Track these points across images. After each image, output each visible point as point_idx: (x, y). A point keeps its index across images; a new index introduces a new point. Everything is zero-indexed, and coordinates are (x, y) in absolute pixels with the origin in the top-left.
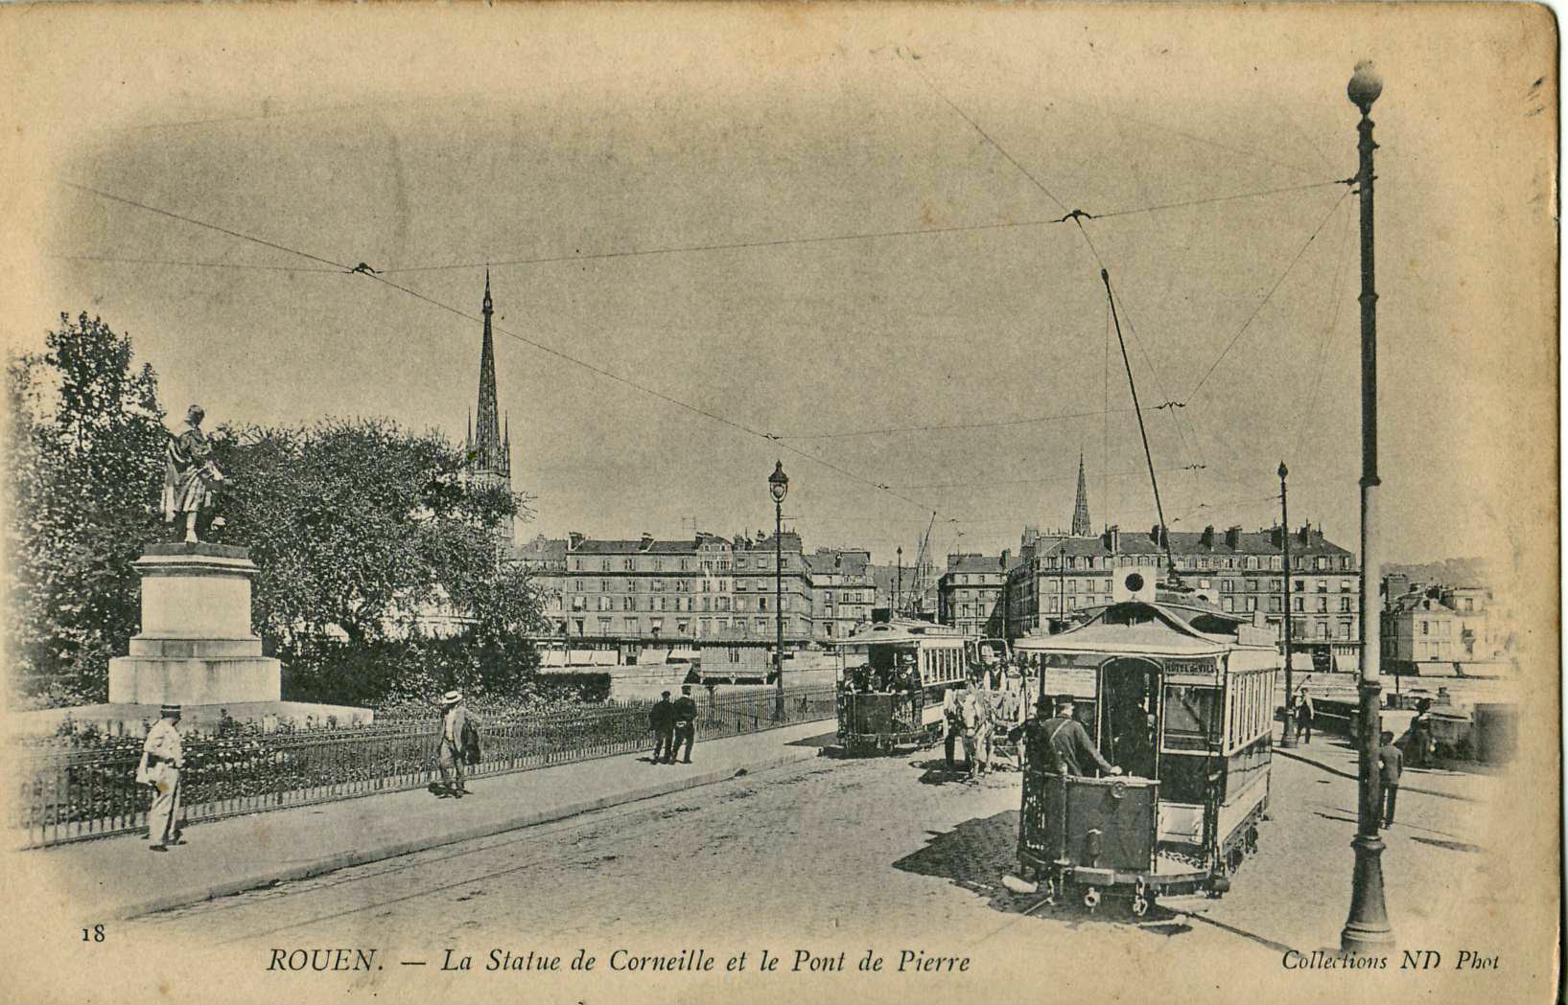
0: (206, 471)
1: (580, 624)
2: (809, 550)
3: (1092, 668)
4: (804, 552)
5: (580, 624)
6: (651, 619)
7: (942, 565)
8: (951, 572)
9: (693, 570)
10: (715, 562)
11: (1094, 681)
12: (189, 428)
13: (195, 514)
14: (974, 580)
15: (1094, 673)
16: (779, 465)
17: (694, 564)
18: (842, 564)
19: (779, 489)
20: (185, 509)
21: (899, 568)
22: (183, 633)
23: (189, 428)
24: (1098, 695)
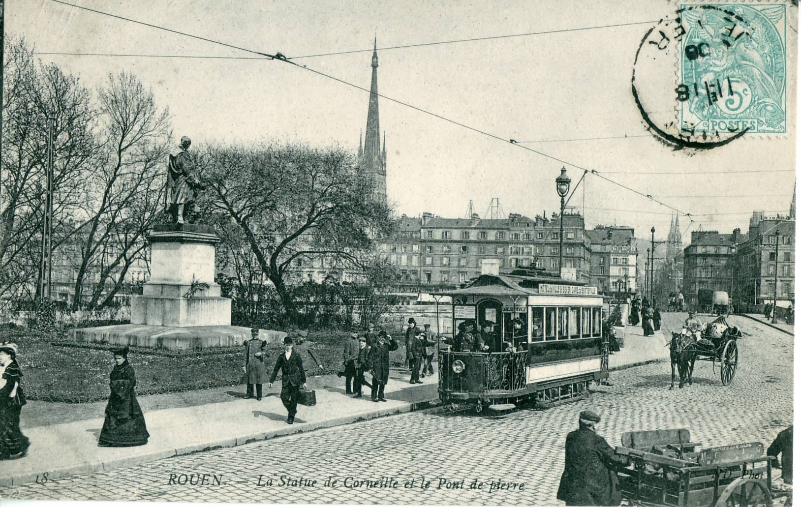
0: (190, 178)
1: (429, 276)
2: (589, 227)
3: (473, 305)
4: (586, 228)
5: (429, 276)
6: (441, 272)
7: (687, 240)
8: (694, 243)
9: (507, 239)
10: (521, 234)
11: (474, 312)
12: (181, 151)
13: (183, 206)
14: (711, 250)
15: (474, 308)
16: (563, 171)
17: (509, 236)
18: (613, 238)
19: (564, 187)
20: (178, 202)
21: (653, 242)
22: (174, 281)
23: (181, 151)
24: (476, 317)
